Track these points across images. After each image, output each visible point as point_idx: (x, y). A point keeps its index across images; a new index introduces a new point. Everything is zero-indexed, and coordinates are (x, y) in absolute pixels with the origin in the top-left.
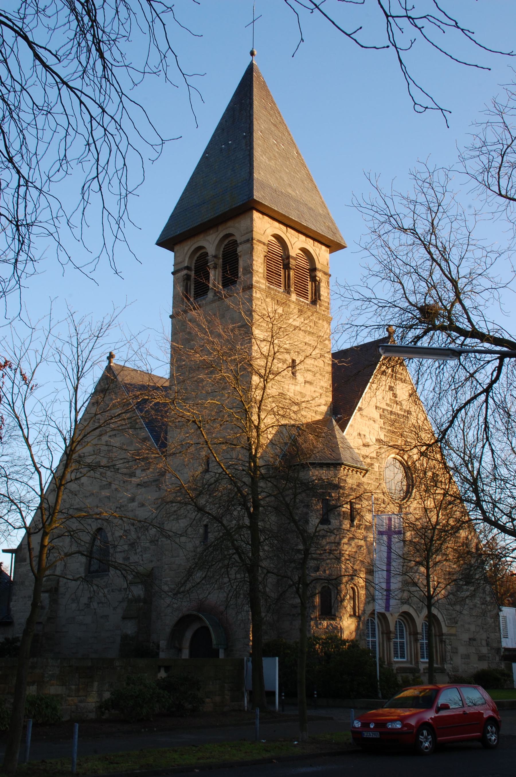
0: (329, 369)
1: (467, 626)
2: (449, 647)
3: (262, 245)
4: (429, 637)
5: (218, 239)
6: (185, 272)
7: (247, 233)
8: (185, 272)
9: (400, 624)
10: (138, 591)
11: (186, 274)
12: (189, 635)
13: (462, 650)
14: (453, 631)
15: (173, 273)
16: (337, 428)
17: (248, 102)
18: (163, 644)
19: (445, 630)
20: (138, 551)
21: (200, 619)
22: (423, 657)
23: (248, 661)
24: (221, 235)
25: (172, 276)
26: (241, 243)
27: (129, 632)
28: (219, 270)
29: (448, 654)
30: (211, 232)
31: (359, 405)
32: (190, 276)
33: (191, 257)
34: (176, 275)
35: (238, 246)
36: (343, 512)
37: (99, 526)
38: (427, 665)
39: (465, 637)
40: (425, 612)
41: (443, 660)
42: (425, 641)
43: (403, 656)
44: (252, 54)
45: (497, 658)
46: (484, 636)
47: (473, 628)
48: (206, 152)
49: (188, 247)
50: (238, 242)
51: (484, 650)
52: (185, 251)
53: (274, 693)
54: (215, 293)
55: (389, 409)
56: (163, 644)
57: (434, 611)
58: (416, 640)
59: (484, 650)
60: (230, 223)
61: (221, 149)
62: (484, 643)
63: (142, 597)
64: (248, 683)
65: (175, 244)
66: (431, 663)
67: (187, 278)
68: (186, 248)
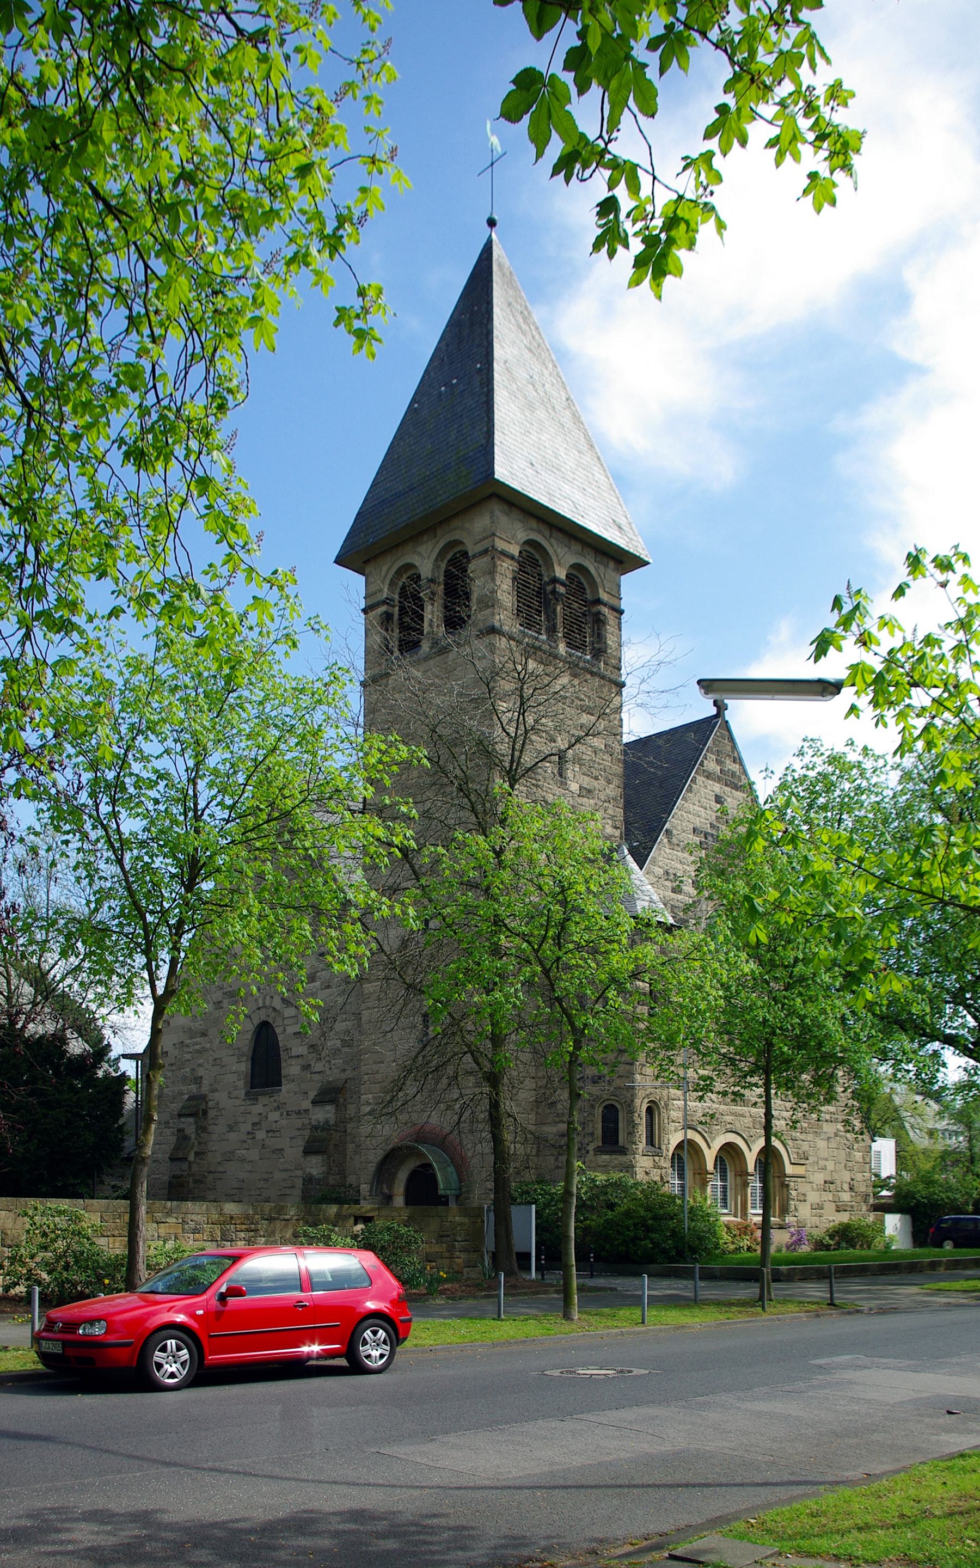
0: (618, 769)
1: (822, 1163)
2: (794, 1193)
3: (510, 562)
4: (764, 1180)
5: (437, 551)
6: (383, 608)
7: (484, 539)
8: (383, 608)
9: (722, 1160)
10: (325, 1114)
11: (386, 612)
12: (402, 1176)
13: (813, 1197)
14: (800, 1170)
15: (365, 611)
16: (633, 865)
17: (483, 310)
18: (365, 1188)
19: (789, 1169)
20: (323, 1054)
21: (420, 1155)
22: (754, 1207)
23: (489, 1210)
24: (442, 544)
25: (363, 616)
26: (474, 557)
27: (315, 1172)
28: (439, 602)
29: (792, 1202)
30: (425, 538)
31: (667, 826)
32: (392, 615)
33: (392, 584)
34: (370, 614)
35: (469, 561)
36: (832, 1075)
37: (264, 1018)
38: (760, 1218)
39: (819, 1178)
40: (761, 1143)
41: (784, 1211)
42: (758, 1185)
43: (725, 1207)
44: (492, 223)
45: (864, 1208)
46: (847, 1176)
47: (830, 1165)
48: (413, 401)
49: (388, 568)
50: (470, 554)
51: (846, 1197)
52: (383, 573)
53: (529, 1254)
54: (435, 643)
55: (714, 832)
56: (365, 1188)
57: (776, 1143)
58: (746, 1184)
59: (846, 1197)
60: (456, 523)
61: (440, 394)
62: (846, 1187)
63: (332, 1122)
64: (489, 1243)
65: (367, 562)
66: (766, 1216)
67: (388, 617)
68: (385, 568)
